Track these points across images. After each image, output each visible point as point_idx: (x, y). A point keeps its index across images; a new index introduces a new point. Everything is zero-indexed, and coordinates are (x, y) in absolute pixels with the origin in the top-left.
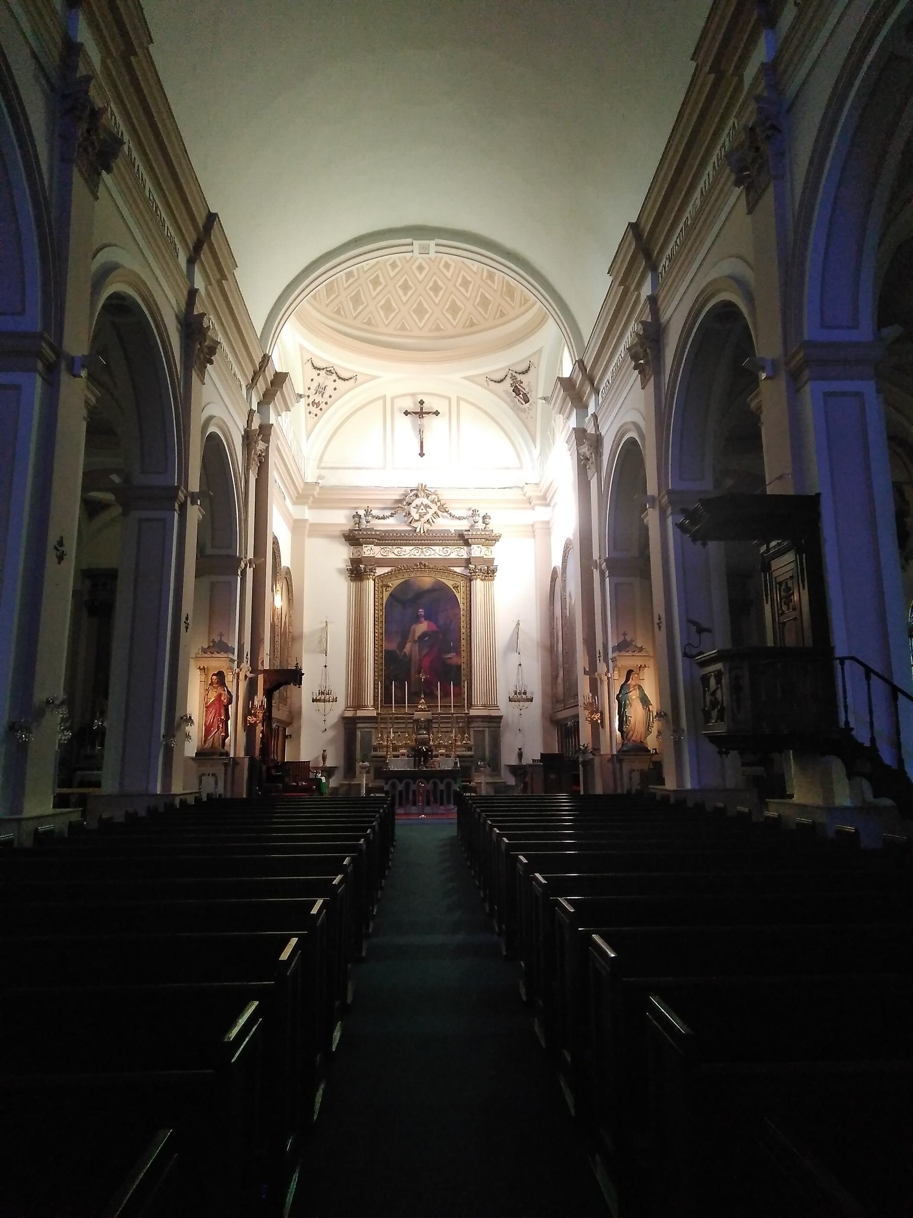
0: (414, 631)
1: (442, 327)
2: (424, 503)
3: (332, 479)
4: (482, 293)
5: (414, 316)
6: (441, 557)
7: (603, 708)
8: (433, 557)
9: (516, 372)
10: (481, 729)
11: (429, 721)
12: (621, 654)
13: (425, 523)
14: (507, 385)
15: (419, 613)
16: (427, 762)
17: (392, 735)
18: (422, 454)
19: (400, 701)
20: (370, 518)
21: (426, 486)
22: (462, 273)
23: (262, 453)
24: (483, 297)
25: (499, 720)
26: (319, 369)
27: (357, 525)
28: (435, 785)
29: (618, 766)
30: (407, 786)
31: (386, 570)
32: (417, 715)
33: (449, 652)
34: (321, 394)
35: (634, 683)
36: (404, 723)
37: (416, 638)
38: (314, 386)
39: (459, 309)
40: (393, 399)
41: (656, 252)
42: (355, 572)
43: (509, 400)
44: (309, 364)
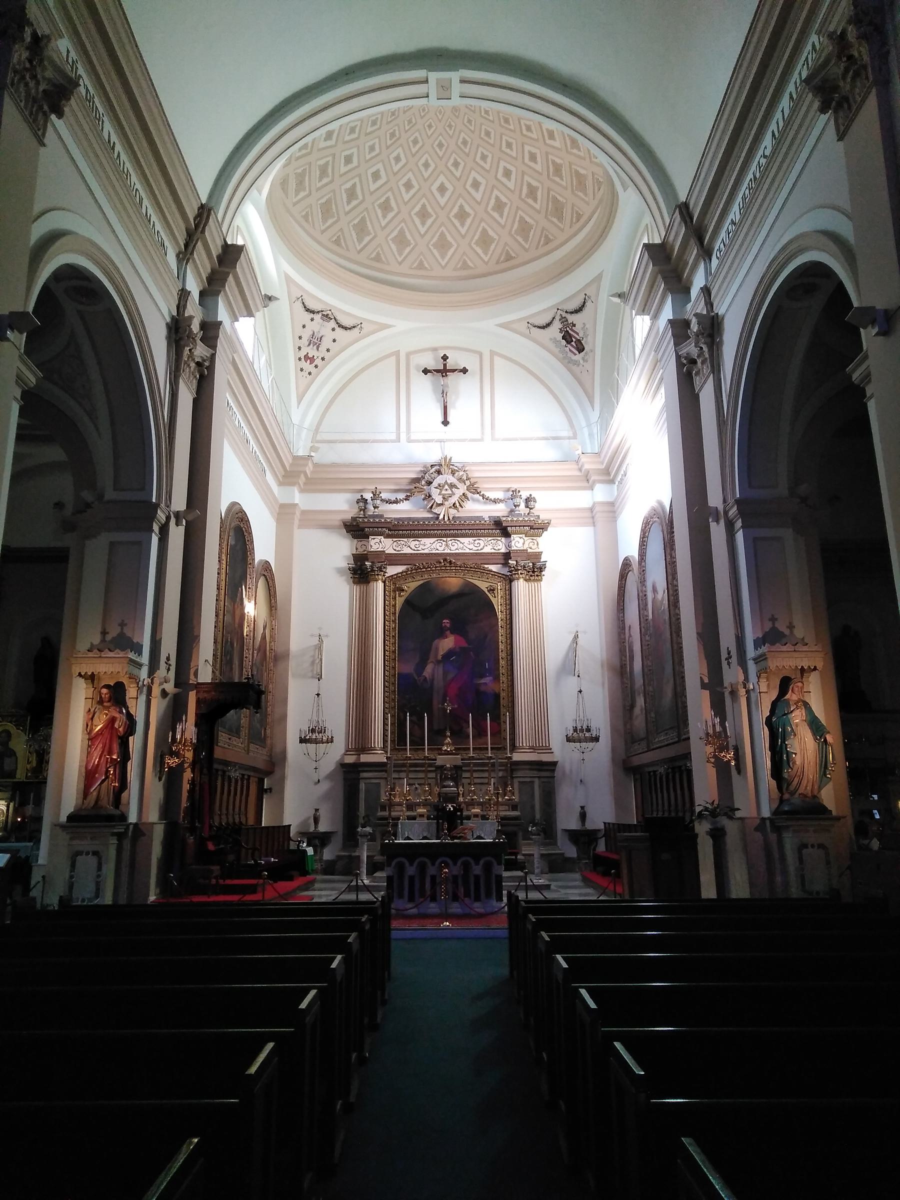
0: (437, 649)
1: (470, 264)
2: (449, 482)
3: (326, 456)
4: (521, 217)
5: (435, 251)
6: (471, 551)
7: (739, 737)
8: (460, 551)
9: (566, 312)
10: (528, 780)
11: (457, 768)
12: (773, 648)
13: (450, 507)
14: (555, 331)
15: (443, 625)
16: (456, 828)
17: (406, 788)
18: (445, 423)
19: (417, 743)
20: (378, 502)
21: (450, 459)
22: (496, 192)
23: (204, 361)
24: (522, 221)
25: (553, 768)
26: (313, 312)
27: (362, 512)
28: (466, 867)
29: (773, 837)
30: (422, 868)
31: (399, 569)
32: (441, 760)
33: (482, 676)
34: (315, 346)
35: (795, 697)
36: (423, 771)
37: (440, 657)
38: (306, 335)
39: (492, 240)
40: (408, 355)
41: (707, 238)
42: (359, 572)
43: (557, 350)
44: (299, 304)
